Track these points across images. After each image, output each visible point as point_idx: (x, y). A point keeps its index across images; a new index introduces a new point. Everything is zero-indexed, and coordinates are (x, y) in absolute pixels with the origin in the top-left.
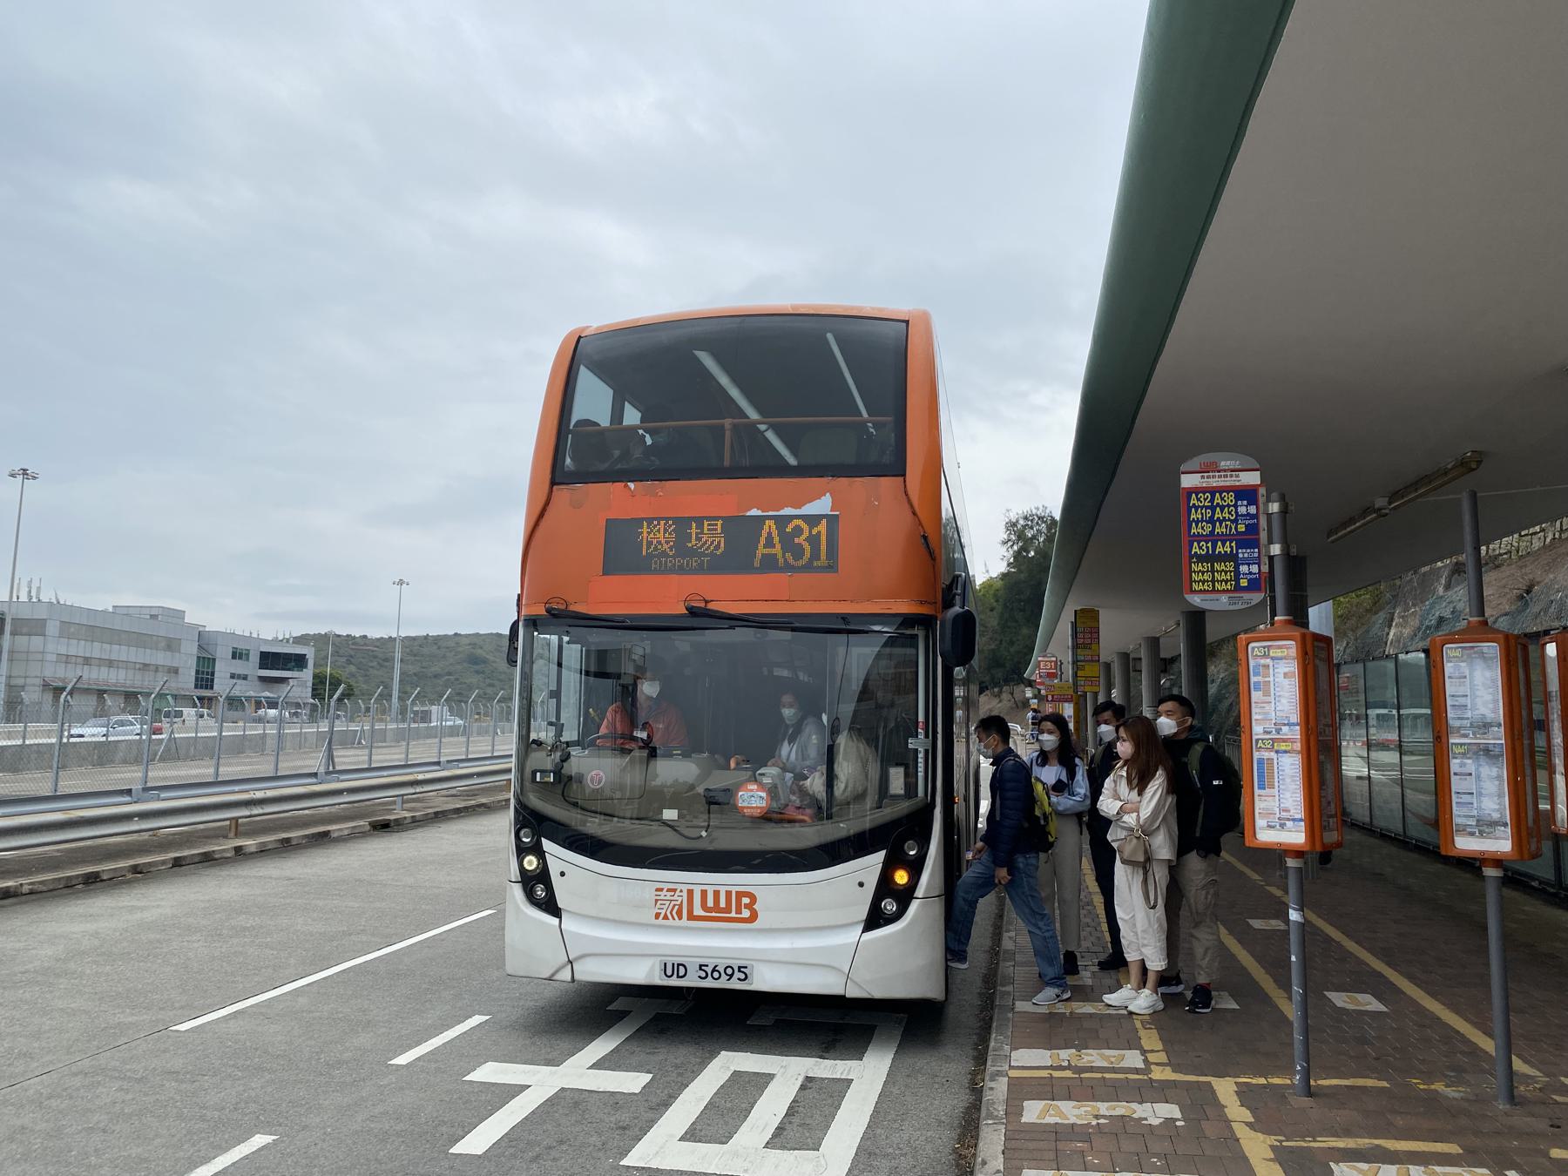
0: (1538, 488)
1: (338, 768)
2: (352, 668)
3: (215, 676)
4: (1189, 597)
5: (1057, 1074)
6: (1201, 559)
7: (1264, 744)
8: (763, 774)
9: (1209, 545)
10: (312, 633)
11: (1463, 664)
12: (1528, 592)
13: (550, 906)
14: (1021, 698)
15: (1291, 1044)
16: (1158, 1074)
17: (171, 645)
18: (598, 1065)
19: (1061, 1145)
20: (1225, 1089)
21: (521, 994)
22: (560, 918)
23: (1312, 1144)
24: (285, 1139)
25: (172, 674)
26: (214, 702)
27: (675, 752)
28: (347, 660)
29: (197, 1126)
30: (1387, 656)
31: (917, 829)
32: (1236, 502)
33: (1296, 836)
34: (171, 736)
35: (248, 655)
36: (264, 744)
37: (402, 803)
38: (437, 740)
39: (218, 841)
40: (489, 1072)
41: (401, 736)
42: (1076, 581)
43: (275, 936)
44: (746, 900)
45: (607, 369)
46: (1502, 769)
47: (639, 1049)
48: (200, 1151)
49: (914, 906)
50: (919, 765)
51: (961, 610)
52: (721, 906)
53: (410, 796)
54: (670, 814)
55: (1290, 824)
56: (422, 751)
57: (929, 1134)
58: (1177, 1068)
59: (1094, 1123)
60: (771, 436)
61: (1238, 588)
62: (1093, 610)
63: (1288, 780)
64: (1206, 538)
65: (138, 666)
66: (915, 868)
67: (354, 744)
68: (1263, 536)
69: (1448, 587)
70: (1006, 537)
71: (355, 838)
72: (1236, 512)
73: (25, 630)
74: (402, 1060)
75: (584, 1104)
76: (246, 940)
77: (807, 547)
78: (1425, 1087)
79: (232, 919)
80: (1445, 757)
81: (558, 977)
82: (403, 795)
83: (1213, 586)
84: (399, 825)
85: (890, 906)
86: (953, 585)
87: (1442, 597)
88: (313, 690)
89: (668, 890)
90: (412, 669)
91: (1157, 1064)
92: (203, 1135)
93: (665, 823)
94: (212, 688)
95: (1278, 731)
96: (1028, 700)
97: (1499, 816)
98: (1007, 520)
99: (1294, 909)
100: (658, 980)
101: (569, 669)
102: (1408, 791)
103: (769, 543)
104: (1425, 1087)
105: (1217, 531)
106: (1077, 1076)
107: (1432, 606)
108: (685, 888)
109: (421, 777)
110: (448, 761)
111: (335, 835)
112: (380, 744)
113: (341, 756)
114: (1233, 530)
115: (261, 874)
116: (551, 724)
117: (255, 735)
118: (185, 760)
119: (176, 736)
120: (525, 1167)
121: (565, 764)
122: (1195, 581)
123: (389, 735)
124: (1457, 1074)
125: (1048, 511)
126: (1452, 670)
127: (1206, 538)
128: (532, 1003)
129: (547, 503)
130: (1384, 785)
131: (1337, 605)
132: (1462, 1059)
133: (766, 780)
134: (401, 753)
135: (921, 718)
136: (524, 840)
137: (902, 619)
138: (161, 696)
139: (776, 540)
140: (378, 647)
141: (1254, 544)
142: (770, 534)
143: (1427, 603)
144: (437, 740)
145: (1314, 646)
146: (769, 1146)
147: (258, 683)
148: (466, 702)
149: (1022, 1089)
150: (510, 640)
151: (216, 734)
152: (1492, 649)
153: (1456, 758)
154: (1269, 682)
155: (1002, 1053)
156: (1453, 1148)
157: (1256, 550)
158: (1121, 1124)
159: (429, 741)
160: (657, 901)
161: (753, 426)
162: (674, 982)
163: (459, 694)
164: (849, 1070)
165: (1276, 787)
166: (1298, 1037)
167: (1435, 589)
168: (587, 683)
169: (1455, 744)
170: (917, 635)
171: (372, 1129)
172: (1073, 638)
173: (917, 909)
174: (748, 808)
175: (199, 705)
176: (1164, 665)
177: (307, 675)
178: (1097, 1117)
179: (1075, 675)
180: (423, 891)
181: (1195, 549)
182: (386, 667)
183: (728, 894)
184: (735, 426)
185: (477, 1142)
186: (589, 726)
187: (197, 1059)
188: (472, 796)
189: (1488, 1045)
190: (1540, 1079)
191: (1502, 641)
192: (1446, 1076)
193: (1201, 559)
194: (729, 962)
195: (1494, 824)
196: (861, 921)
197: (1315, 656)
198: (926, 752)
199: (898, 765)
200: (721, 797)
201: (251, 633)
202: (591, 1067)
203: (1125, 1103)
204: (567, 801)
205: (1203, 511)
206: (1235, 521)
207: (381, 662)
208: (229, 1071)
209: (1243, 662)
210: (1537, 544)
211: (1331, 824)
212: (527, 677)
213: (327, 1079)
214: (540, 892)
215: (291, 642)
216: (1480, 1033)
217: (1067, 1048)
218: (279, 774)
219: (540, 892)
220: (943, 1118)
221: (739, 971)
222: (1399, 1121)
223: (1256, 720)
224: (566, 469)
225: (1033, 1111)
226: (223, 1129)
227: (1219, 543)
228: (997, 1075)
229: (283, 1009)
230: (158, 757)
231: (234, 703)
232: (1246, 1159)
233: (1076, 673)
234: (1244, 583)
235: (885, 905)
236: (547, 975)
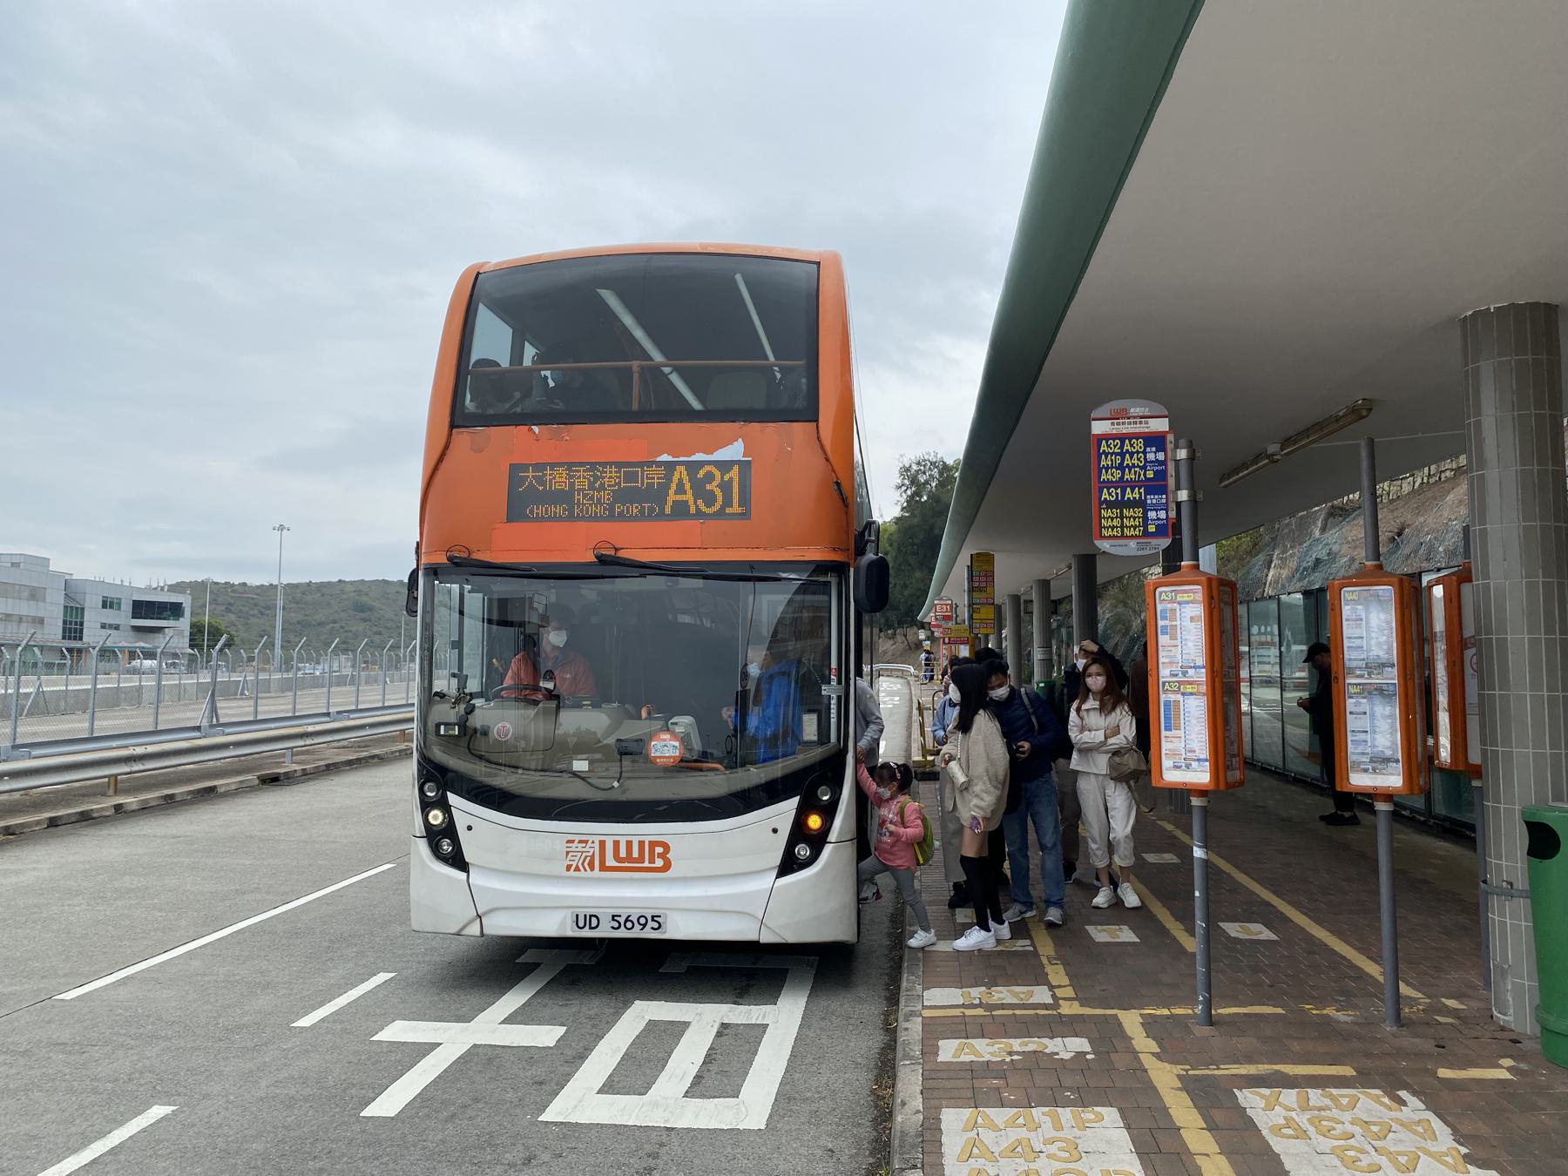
0: (1420, 435)
1: (222, 720)
2: (232, 617)
3: (85, 625)
4: (1098, 543)
5: (969, 1012)
6: (1110, 505)
8: (676, 724)
9: (1119, 491)
11: (1360, 607)
12: (1399, 534)
13: (457, 861)
14: (914, 640)
15: (1194, 976)
16: (1067, 1009)
17: (35, 595)
18: (509, 1020)
19: (977, 1083)
20: (1131, 1021)
21: (426, 949)
22: (468, 872)
23: (1216, 1072)
24: (185, 1109)
25: (37, 625)
26: (83, 655)
27: (584, 703)
29: (89, 1099)
30: (1270, 597)
31: (829, 774)
32: (1145, 449)
33: (1201, 776)
34: (39, 689)
35: (119, 604)
36: (140, 696)
37: (292, 756)
38: (325, 690)
39: (95, 799)
40: (398, 1031)
41: (287, 686)
42: (973, 526)
43: (163, 897)
44: (659, 850)
45: (506, 309)
46: (1395, 707)
47: (551, 1001)
48: (93, 1126)
49: (827, 850)
50: (832, 711)
51: (875, 557)
52: (621, 856)
53: (299, 749)
54: (580, 765)
55: (1195, 764)
56: (310, 702)
57: (847, 1076)
58: (1084, 1002)
59: (1008, 1059)
60: (675, 379)
61: (1146, 534)
62: (987, 555)
64: (1115, 485)
66: (829, 812)
68: (1171, 482)
69: (1323, 530)
70: (899, 481)
71: (241, 792)
72: (1145, 459)
73: (29, 618)
74: (306, 1022)
75: (498, 1060)
76: (131, 902)
77: (718, 493)
78: (1317, 1012)
79: (115, 880)
80: (1342, 698)
81: (465, 932)
83: (1122, 531)
84: (289, 778)
85: (803, 851)
86: (863, 533)
87: (1318, 540)
88: (190, 640)
89: (580, 842)
90: (295, 617)
91: (1065, 999)
92: (96, 1108)
93: (575, 774)
94: (81, 639)
95: (1185, 674)
96: (921, 641)
97: (1391, 753)
98: (902, 465)
99: (1199, 847)
100: (570, 932)
101: (471, 617)
102: (1288, 726)
103: (681, 489)
104: (1317, 1012)
105: (1126, 477)
106: (989, 1013)
107: (1310, 548)
108: (597, 839)
109: (310, 729)
110: (338, 713)
111: (222, 790)
112: (264, 695)
113: (225, 708)
114: (1142, 476)
115: (144, 833)
116: (454, 675)
117: (130, 687)
119: (45, 689)
120: (440, 1127)
121: (469, 716)
122: (1105, 527)
124: (1347, 999)
125: (939, 456)
126: (1349, 613)
127: (1115, 485)
128: (438, 959)
129: (447, 447)
130: (1266, 721)
131: (1220, 547)
132: (1349, 984)
133: (678, 729)
134: (289, 704)
135: (834, 665)
136: (429, 794)
137: (814, 566)
138: (28, 647)
139: (688, 486)
140: (258, 595)
141: (1162, 490)
142: (680, 480)
143: (1305, 545)
144: (325, 690)
145: (1219, 591)
146: (689, 1095)
147: (131, 633)
148: (354, 651)
149: (936, 1030)
150: (409, 590)
151: (90, 687)
152: (1387, 592)
153: (1352, 698)
155: (914, 993)
156: (1348, 1071)
157: (1164, 496)
158: (1034, 1059)
159: (316, 691)
160: (568, 853)
161: (656, 370)
162: (586, 933)
163: (344, 643)
164: (764, 1016)
165: (1182, 728)
166: (1200, 969)
167: (1312, 531)
168: (489, 631)
169: (1351, 684)
170: (830, 582)
171: (278, 1095)
172: (969, 583)
173: (830, 855)
174: (660, 757)
176: (1053, 607)
177: (184, 623)
178: (1010, 1053)
179: (971, 618)
180: (317, 846)
181: (1105, 496)
182: (268, 615)
183: (641, 844)
184: (642, 370)
185: (390, 1103)
186: (492, 677)
187: (86, 1028)
188: (365, 747)
189: (1373, 969)
190: (1421, 1000)
191: (1397, 584)
192: (1337, 1001)
193: (1110, 505)
194: (643, 912)
195: (1387, 760)
196: (775, 868)
197: (1220, 600)
198: (839, 698)
199: (810, 711)
200: (632, 747)
201: (122, 581)
202: (503, 1022)
203: (1036, 1039)
204: (471, 753)
205: (1113, 458)
206: (1144, 468)
207: (262, 610)
208: (121, 1040)
209: (1151, 607)
210: (1406, 488)
211: (1234, 763)
212: (428, 627)
213: (227, 1045)
214: (446, 846)
215: (166, 590)
216: (1364, 958)
217: (977, 986)
218: (159, 728)
219: (446, 846)
220: (859, 1060)
221: (653, 920)
222: (1296, 1046)
223: (1163, 663)
224: (467, 411)
225: (948, 1050)
226: (118, 1101)
227: (1129, 489)
228: (911, 1015)
229: (174, 973)
230: (26, 711)
231: (107, 653)
232: (1154, 1089)
233: (972, 616)
234: (1152, 529)
235: (798, 851)
236: (454, 931)
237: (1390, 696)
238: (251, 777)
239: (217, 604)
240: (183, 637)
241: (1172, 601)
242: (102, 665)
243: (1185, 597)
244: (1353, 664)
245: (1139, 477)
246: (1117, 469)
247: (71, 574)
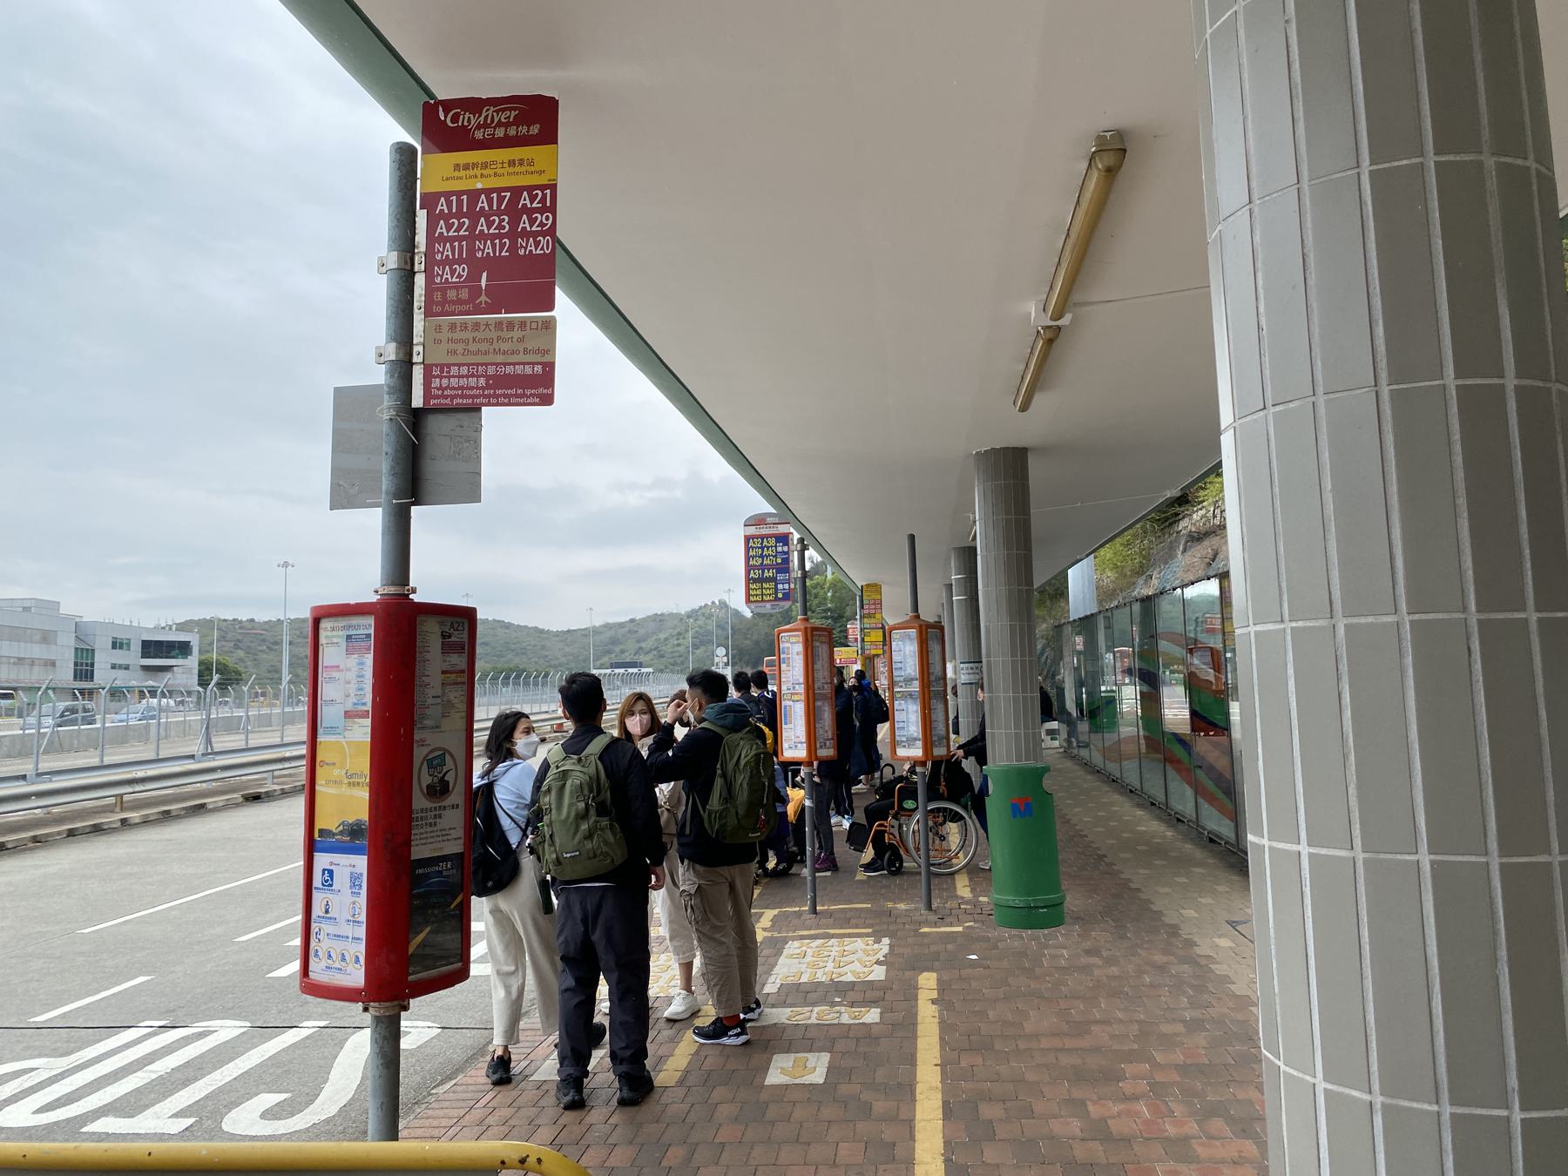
2: (241, 653)
10: (196, 619)
17: (47, 638)
28: (235, 645)
35: (129, 645)
55: (799, 745)
61: (777, 599)
62: (876, 585)
65: (12, 661)
67: (239, 729)
82: (273, 771)
95: (794, 688)
109: (288, 754)
111: (211, 806)
112: (265, 729)
118: (69, 751)
123: (275, 720)
140: (266, 630)
147: (141, 673)
154: (1409, 614)
175: (80, 698)
177: (192, 662)
182: (276, 650)
201: (131, 622)
206: (775, 556)
207: (271, 645)
215: (174, 629)
218: (160, 757)
231: (116, 693)
234: (780, 595)
237: (915, 699)
238: (237, 796)
239: (226, 641)
240: (192, 674)
241: (788, 642)
242: (113, 705)
244: (898, 679)
246: (759, 557)
247: (81, 617)
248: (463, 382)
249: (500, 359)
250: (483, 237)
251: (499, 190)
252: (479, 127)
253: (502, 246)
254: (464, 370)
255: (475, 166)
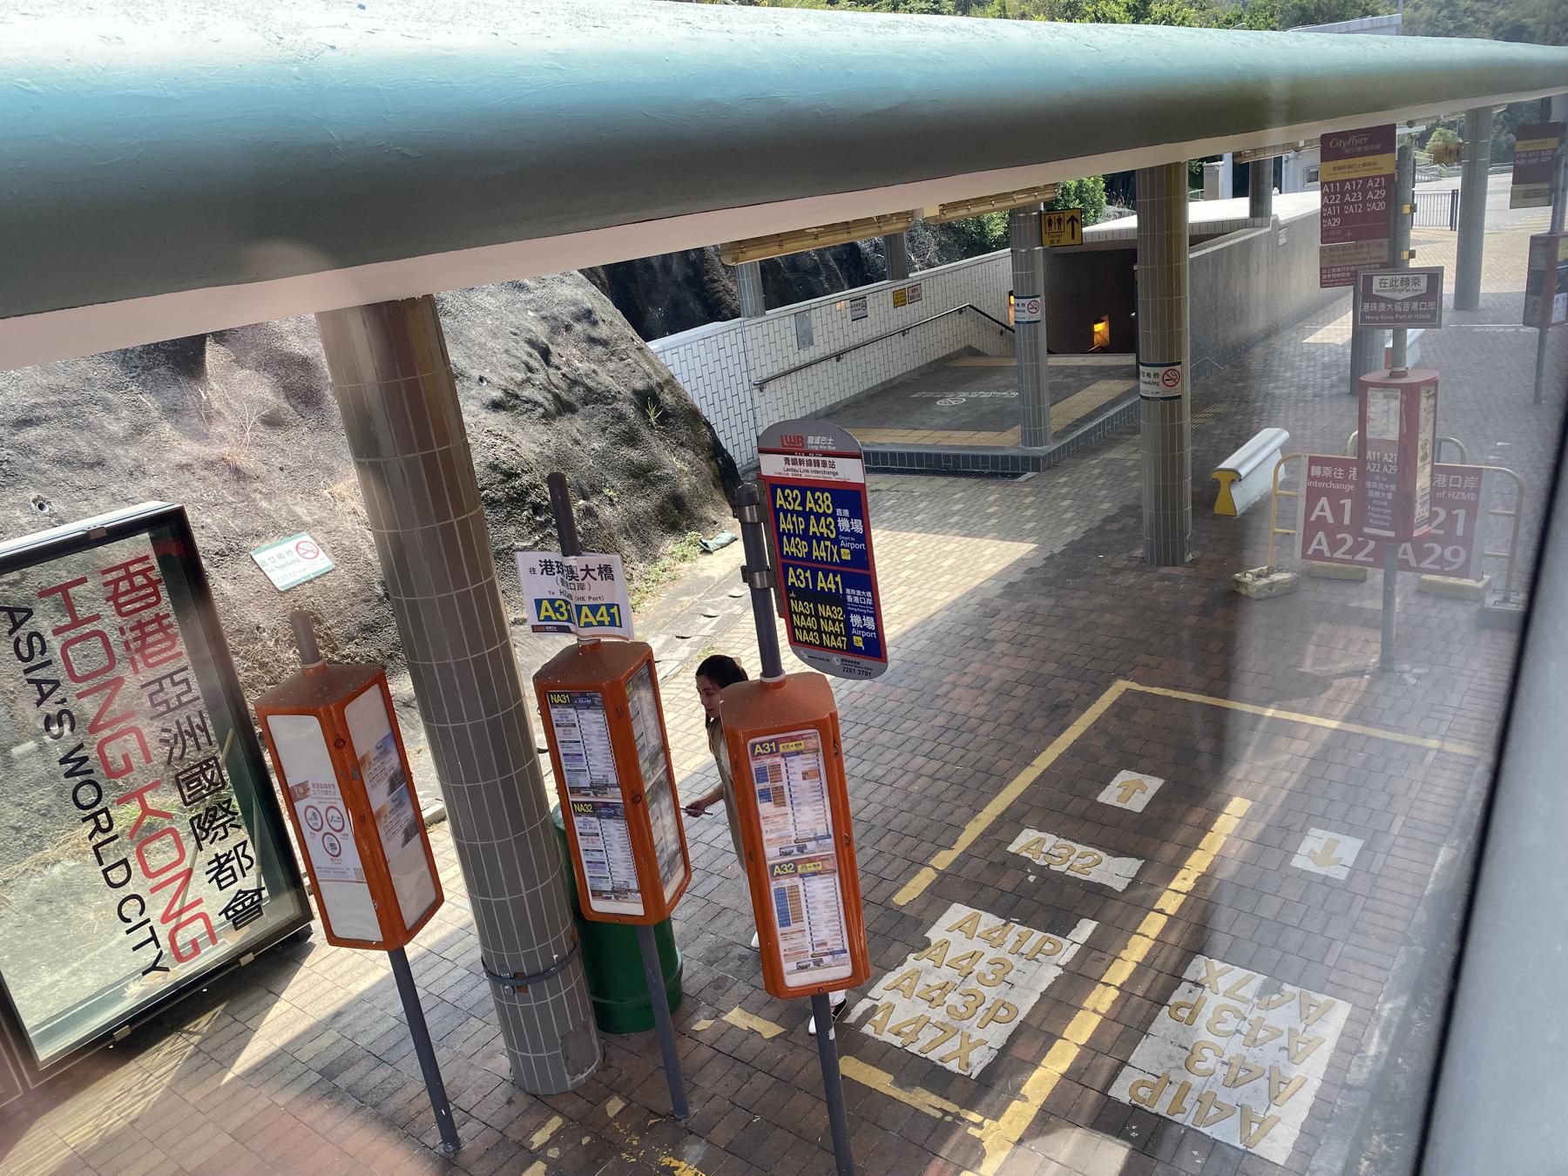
7: (782, 869)
9: (808, 574)
32: (834, 511)
55: (827, 959)
63: (820, 906)
95: (801, 850)
114: (835, 556)
243: (792, 747)
245: (832, 558)
248: (1338, 275)
249: (1344, 264)
250: (1348, 203)
251: (1356, 179)
252: (1347, 147)
253: (1359, 207)
254: (1339, 270)
255: (1344, 167)
